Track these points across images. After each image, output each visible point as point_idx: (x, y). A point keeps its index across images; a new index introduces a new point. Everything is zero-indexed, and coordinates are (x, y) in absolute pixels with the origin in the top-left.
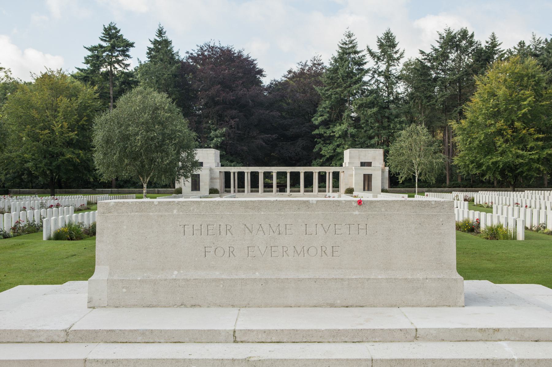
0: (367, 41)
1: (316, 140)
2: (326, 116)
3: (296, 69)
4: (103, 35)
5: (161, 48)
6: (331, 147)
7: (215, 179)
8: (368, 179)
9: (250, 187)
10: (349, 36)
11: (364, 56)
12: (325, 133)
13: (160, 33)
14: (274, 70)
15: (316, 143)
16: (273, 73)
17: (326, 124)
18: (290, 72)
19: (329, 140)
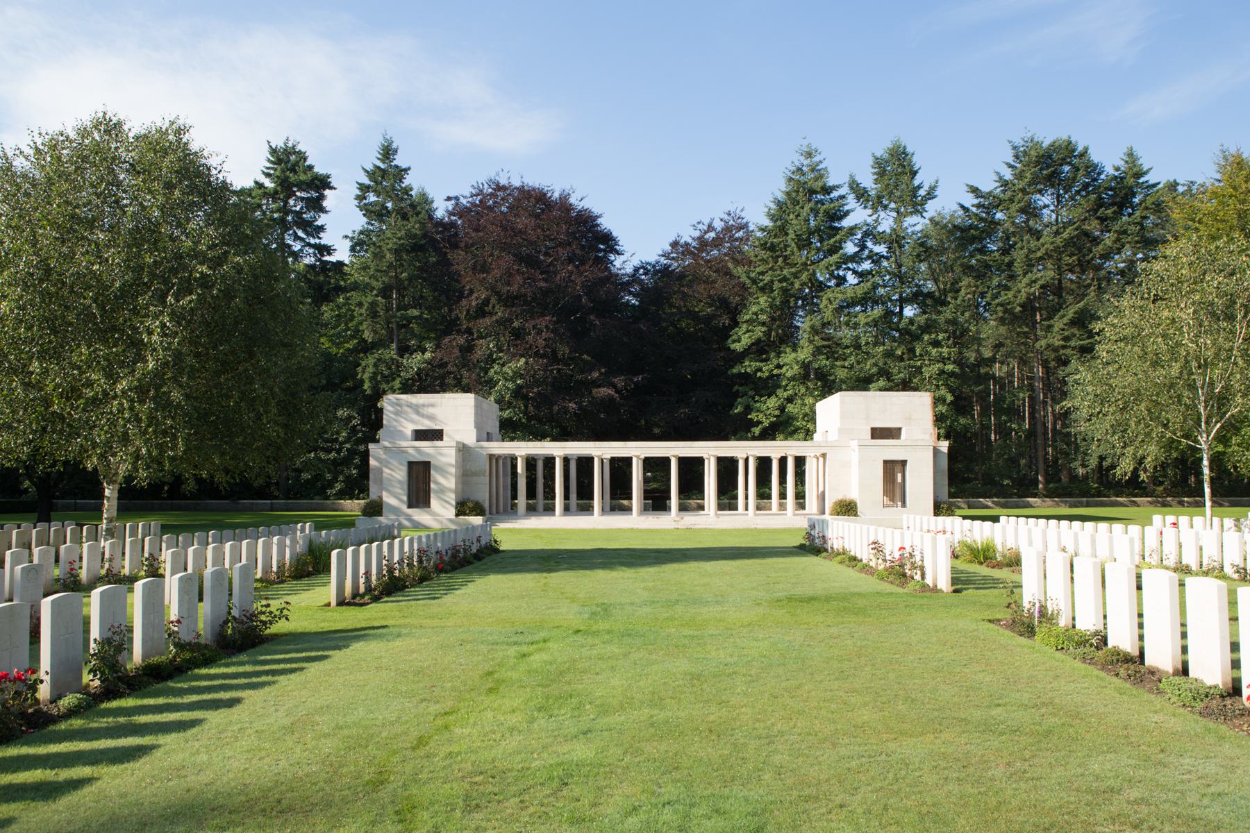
0: (849, 166)
1: (736, 388)
2: (759, 331)
3: (688, 235)
4: (269, 165)
5: (386, 178)
6: (772, 402)
7: (475, 474)
8: (893, 470)
9: (607, 496)
10: (809, 155)
11: (842, 197)
12: (760, 370)
13: (388, 152)
14: (642, 239)
15: (737, 395)
16: (640, 244)
17: (760, 349)
18: (675, 244)
19: (769, 386)
